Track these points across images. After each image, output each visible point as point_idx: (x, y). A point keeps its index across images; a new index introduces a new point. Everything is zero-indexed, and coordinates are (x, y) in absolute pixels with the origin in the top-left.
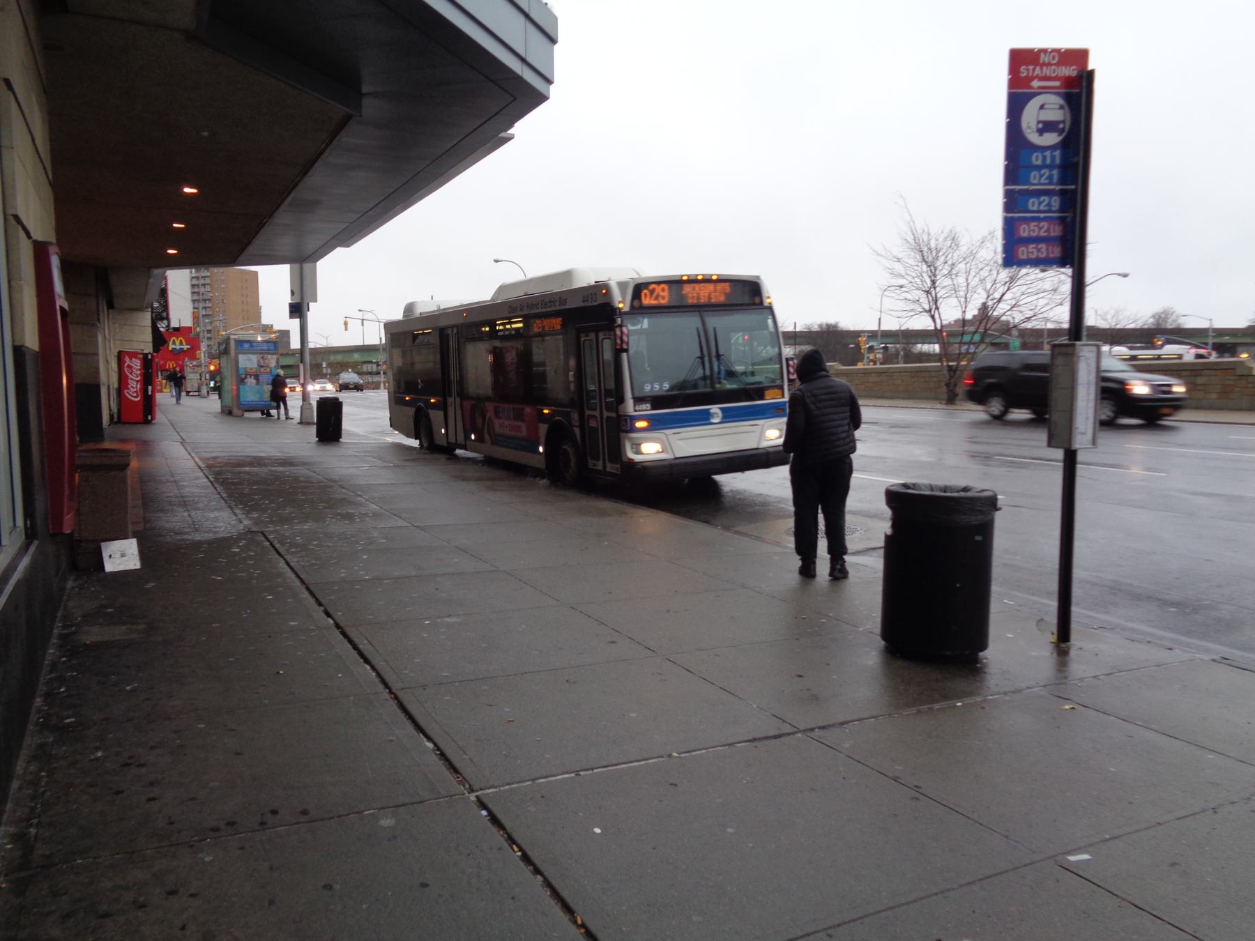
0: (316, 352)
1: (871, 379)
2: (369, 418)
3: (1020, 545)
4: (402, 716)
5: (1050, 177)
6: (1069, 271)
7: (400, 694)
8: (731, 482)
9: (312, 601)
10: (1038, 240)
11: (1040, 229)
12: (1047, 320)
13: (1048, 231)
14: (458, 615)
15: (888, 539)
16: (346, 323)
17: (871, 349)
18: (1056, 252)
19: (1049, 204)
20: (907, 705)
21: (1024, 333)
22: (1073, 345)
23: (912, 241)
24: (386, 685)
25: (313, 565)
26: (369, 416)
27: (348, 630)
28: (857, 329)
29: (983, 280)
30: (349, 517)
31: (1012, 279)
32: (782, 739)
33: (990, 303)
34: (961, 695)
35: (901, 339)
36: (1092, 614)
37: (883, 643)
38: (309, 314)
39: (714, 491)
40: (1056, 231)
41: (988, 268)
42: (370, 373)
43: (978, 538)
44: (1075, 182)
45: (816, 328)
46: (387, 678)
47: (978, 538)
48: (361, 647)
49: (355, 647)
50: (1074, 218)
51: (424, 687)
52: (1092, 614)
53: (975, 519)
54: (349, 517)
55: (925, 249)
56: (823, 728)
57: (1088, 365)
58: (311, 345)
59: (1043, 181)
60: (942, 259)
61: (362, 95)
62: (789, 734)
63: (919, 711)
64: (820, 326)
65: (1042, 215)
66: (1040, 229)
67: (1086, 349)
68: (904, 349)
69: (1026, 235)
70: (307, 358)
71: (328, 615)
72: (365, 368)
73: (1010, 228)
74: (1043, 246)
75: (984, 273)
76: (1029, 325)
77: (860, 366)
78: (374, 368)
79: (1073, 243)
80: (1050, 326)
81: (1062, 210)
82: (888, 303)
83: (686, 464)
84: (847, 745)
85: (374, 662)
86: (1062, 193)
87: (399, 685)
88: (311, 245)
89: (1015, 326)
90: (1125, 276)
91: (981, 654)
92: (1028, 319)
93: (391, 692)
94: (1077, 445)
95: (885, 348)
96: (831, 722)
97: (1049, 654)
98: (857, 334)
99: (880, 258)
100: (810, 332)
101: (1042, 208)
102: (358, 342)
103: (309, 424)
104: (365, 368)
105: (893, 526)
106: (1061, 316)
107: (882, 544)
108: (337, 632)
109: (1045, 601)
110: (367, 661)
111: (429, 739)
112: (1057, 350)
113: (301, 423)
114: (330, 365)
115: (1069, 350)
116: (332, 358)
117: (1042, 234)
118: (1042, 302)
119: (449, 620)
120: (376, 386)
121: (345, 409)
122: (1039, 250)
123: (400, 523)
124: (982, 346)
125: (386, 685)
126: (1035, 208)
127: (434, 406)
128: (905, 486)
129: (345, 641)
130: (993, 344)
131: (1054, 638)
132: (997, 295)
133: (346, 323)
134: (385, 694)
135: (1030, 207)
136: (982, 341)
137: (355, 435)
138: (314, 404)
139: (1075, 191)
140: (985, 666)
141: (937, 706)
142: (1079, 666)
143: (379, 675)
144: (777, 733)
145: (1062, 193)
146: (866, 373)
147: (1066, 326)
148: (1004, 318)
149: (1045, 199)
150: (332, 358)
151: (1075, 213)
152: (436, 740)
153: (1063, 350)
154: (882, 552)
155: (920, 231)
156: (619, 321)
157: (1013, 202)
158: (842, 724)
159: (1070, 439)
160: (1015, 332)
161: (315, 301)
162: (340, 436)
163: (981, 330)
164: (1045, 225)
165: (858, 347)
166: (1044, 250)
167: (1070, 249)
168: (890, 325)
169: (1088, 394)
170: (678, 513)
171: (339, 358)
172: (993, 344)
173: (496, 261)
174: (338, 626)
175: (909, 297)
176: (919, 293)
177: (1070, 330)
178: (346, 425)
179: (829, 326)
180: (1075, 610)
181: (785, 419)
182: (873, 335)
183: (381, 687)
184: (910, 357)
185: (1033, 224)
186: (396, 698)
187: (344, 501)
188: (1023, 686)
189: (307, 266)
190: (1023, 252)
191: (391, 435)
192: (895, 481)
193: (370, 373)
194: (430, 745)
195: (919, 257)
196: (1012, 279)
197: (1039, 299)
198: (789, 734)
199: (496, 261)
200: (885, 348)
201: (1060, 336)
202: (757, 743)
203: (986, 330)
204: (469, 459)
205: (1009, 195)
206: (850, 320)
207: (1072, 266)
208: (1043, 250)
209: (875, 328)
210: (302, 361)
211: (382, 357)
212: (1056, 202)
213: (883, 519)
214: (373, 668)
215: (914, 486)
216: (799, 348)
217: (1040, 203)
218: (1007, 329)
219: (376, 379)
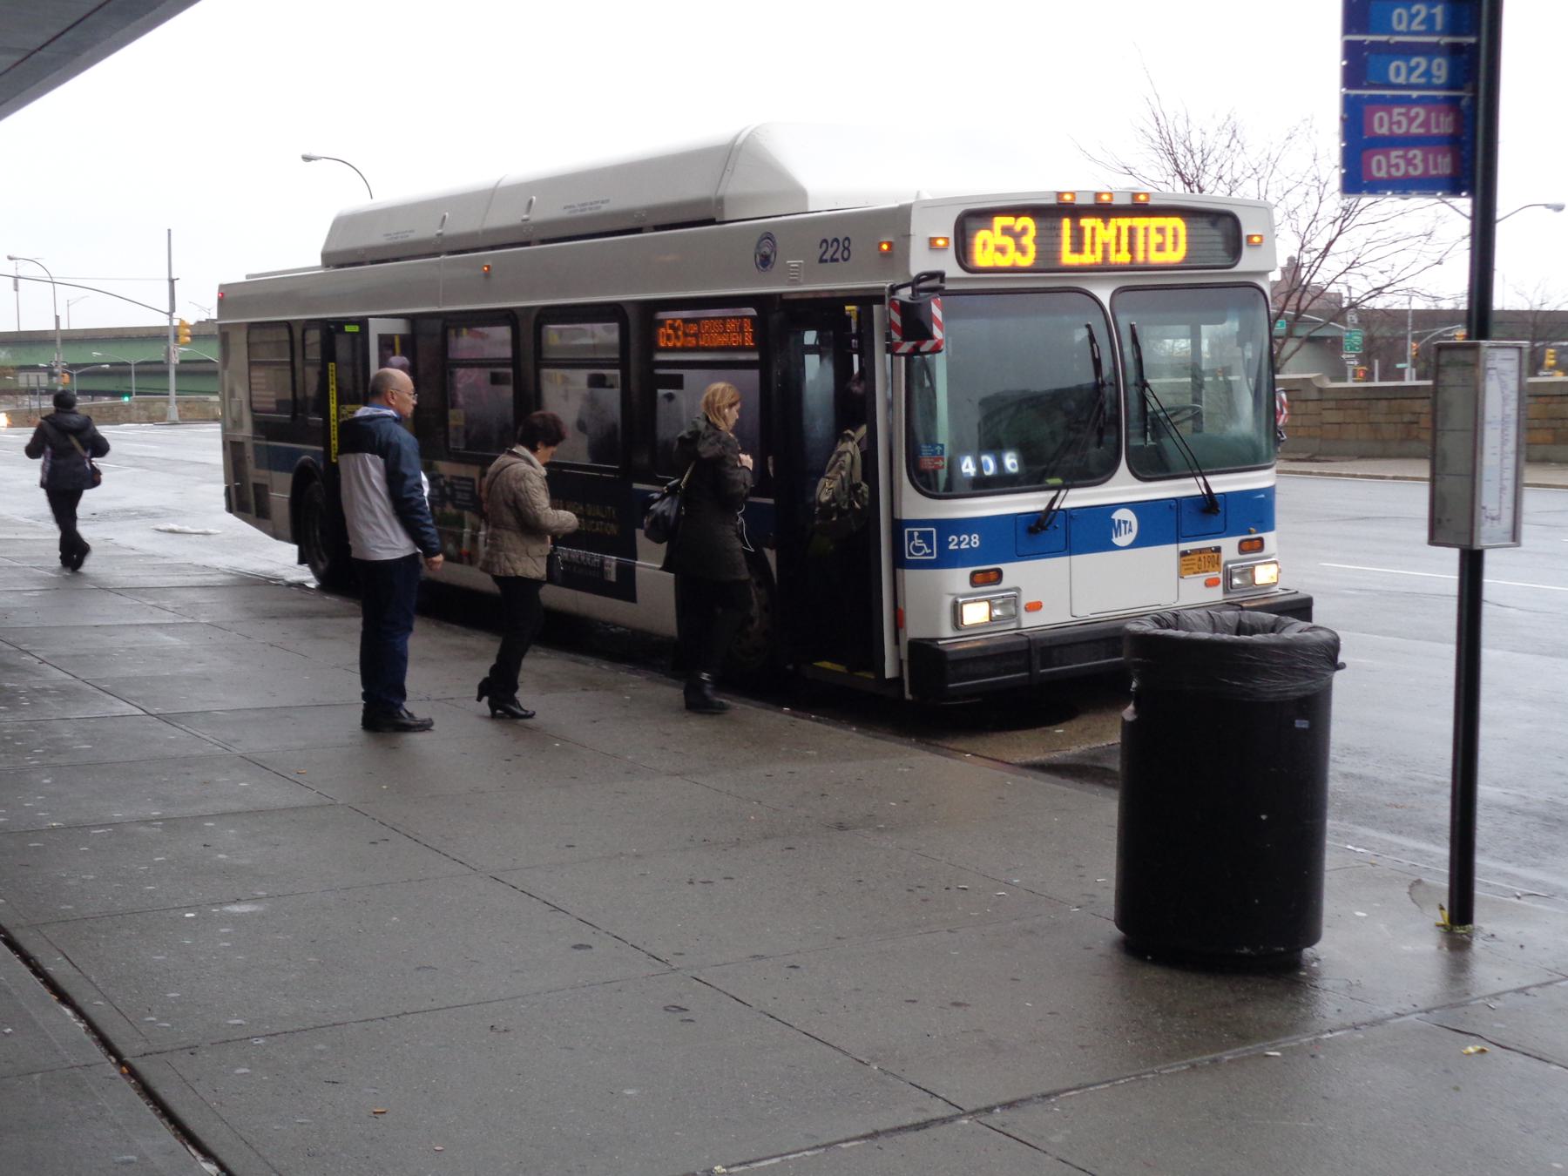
3: (1382, 721)
4: (146, 1110)
5: (1430, 19)
6: (1464, 203)
7: (140, 1065)
10: (1407, 142)
11: (1411, 120)
12: (1411, 293)
13: (1426, 124)
14: (256, 900)
18: (1443, 165)
19: (1427, 73)
20: (1168, 1056)
21: (1370, 319)
22: (1476, 347)
29: (1290, 214)
31: (1347, 212)
32: (931, 1131)
33: (1306, 259)
34: (1275, 1031)
36: (1510, 868)
37: (1117, 933)
40: (1443, 125)
41: (1302, 189)
43: (1301, 724)
44: (1475, 31)
46: (112, 1034)
47: (1301, 724)
48: (50, 969)
49: (38, 971)
50: (1474, 99)
51: (193, 1050)
52: (1510, 868)
53: (1295, 687)
55: (1180, 150)
56: (1009, 1105)
57: (1504, 386)
59: (1415, 27)
60: (1213, 170)
61: (1480, 312)
62: (943, 1121)
63: (1194, 1066)
65: (1415, 94)
66: (1411, 120)
67: (1499, 354)
69: (1384, 131)
72: (23, 380)
73: (1354, 118)
74: (1417, 154)
75: (1294, 200)
76: (1379, 303)
79: (1474, 149)
80: (1419, 304)
81: (1451, 85)
84: (1057, 1139)
85: (80, 1001)
86: (1454, 50)
87: (140, 1047)
89: (1353, 306)
90: (1559, 208)
91: (1307, 952)
92: (1379, 290)
93: (121, 1062)
94: (1482, 542)
96: (1025, 1094)
97: (1434, 948)
101: (1414, 79)
104: (23, 380)
106: (1449, 287)
109: (1423, 846)
110: (64, 998)
111: (208, 1155)
112: (1445, 357)
115: (1468, 356)
117: (1415, 130)
118: (1402, 260)
119: (236, 909)
122: (1409, 162)
123: (126, 708)
124: (1291, 345)
126: (1401, 80)
130: (1310, 340)
131: (1442, 917)
132: (1320, 244)
134: (110, 1067)
135: (1393, 78)
136: (1290, 334)
139: (1476, 46)
140: (1315, 974)
141: (1227, 1056)
142: (1492, 969)
143: (92, 1027)
144: (920, 1118)
145: (1454, 50)
147: (1464, 306)
148: (1333, 289)
149: (1421, 62)
151: (1475, 90)
152: (223, 1157)
153: (1460, 356)
157: (1360, 66)
158: (1046, 1096)
159: (1471, 532)
160: (1352, 317)
163: (1290, 312)
164: (1420, 112)
166: (1418, 161)
167: (1464, 158)
169: (1504, 443)
172: (1310, 340)
173: (307, 159)
177: (1469, 312)
180: (1481, 861)
183: (98, 1052)
185: (1396, 110)
186: (133, 1073)
188: (1389, 1011)
190: (1379, 165)
194: (211, 1168)
195: (1170, 167)
196: (1347, 212)
197: (1406, 254)
198: (943, 1121)
199: (307, 159)
201: (1452, 323)
202: (882, 1141)
203: (1297, 316)
205: (1352, 52)
207: (1472, 194)
208: (1417, 162)
212: (1441, 69)
214: (79, 1013)
216: (854, 321)
217: (1411, 70)
218: (1337, 311)
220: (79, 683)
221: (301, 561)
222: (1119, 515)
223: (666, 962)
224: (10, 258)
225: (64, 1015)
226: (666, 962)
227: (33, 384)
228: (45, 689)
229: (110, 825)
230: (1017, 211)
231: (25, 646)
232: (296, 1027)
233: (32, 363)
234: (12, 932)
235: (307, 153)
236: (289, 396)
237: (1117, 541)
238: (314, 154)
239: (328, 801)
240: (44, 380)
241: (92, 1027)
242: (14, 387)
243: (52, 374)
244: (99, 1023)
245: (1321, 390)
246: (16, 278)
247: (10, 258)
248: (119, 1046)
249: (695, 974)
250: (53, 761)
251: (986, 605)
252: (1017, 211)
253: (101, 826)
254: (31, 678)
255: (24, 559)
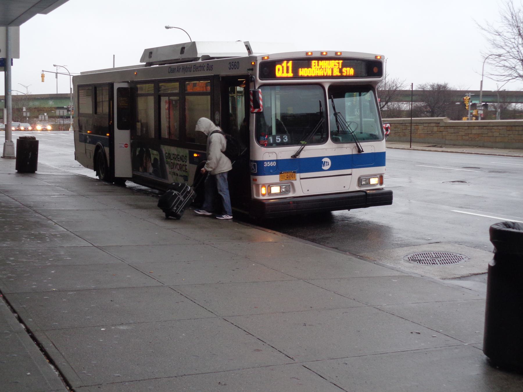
0: (18, 99)
1: (474, 132)
2: (60, 155)
8: (336, 213)
9: (8, 308)
14: (129, 324)
15: (492, 270)
16: (43, 76)
17: (474, 106)
23: (510, 18)
24: (67, 384)
25: (11, 277)
26: (59, 152)
27: (36, 334)
28: (462, 89)
30: (40, 237)
35: (499, 99)
37: (485, 357)
38: (12, 68)
39: (330, 219)
42: (62, 117)
45: (428, 88)
48: (47, 349)
49: (42, 349)
51: (99, 385)
54: (40, 237)
58: (14, 93)
64: (432, 86)
68: (501, 107)
70: (10, 103)
71: (21, 321)
72: (58, 112)
77: (464, 120)
78: (65, 113)
82: (488, 69)
83: (334, 199)
85: (57, 363)
88: (16, 10)
95: (486, 106)
98: (463, 93)
99: (485, 33)
100: (424, 91)
102: (51, 91)
103: (10, 158)
104: (58, 112)
105: (495, 258)
107: (486, 271)
108: (28, 336)
110: (52, 362)
113: (4, 157)
114: (29, 109)
116: (31, 104)
119: (121, 328)
120: (66, 128)
121: (40, 146)
123: (84, 243)
125: (67, 384)
127: (191, 154)
128: (506, 224)
129: (34, 344)
133: (43, 76)
137: (48, 168)
138: (15, 142)
143: (61, 374)
146: (470, 126)
150: (31, 104)
154: (486, 277)
155: (517, 10)
156: (209, 88)
161: (18, 57)
162: (35, 169)
165: (463, 104)
168: (491, 86)
170: (289, 234)
171: (37, 104)
173: (167, 28)
174: (28, 331)
175: (507, 64)
176: (515, 61)
178: (41, 160)
179: (439, 86)
181: (162, 146)
182: (476, 94)
183: (63, 384)
184: (506, 114)
187: (38, 224)
189: (12, 29)
191: (78, 168)
192: (499, 218)
193: (62, 117)
195: (516, 31)
199: (167, 28)
200: (486, 106)
204: (140, 191)
206: (456, 83)
209: (478, 89)
210: (6, 106)
211: (71, 104)
213: (477, 246)
215: (513, 225)
216: (415, 104)
219: (66, 122)
220: (68, 232)
221: (97, 175)
222: (324, 160)
223: (292, 359)
224: (55, 66)
225: (51, 369)
226: (292, 359)
227: (61, 114)
228: (56, 235)
229: (75, 290)
230: (288, 60)
231: (50, 217)
232: (141, 379)
233: (62, 106)
234: (34, 333)
235: (167, 25)
236: (336, 129)
237: (324, 168)
238: (170, 26)
239: (161, 284)
240: (65, 112)
241: (61, 374)
242: (55, 115)
243: (68, 111)
244: (64, 372)
245: (446, 123)
246: (57, 73)
247: (55, 66)
248: (70, 383)
249: (304, 364)
250: (56, 263)
251: (279, 188)
252: (288, 60)
253: (72, 291)
254: (51, 230)
255: (53, 182)
